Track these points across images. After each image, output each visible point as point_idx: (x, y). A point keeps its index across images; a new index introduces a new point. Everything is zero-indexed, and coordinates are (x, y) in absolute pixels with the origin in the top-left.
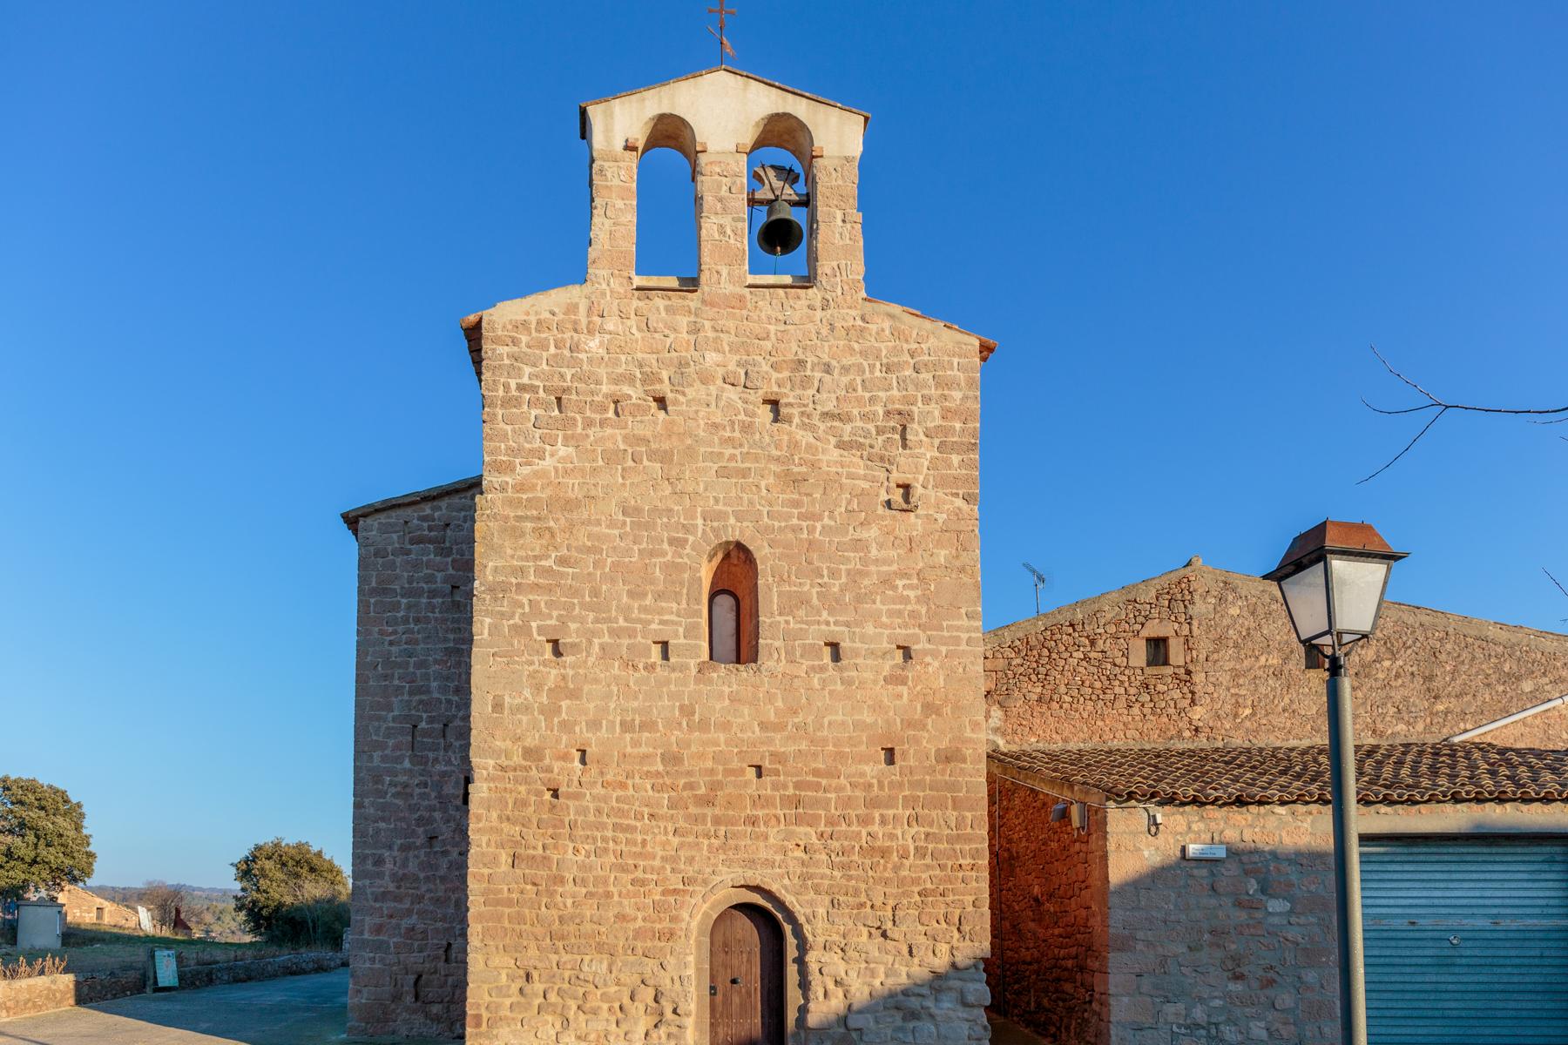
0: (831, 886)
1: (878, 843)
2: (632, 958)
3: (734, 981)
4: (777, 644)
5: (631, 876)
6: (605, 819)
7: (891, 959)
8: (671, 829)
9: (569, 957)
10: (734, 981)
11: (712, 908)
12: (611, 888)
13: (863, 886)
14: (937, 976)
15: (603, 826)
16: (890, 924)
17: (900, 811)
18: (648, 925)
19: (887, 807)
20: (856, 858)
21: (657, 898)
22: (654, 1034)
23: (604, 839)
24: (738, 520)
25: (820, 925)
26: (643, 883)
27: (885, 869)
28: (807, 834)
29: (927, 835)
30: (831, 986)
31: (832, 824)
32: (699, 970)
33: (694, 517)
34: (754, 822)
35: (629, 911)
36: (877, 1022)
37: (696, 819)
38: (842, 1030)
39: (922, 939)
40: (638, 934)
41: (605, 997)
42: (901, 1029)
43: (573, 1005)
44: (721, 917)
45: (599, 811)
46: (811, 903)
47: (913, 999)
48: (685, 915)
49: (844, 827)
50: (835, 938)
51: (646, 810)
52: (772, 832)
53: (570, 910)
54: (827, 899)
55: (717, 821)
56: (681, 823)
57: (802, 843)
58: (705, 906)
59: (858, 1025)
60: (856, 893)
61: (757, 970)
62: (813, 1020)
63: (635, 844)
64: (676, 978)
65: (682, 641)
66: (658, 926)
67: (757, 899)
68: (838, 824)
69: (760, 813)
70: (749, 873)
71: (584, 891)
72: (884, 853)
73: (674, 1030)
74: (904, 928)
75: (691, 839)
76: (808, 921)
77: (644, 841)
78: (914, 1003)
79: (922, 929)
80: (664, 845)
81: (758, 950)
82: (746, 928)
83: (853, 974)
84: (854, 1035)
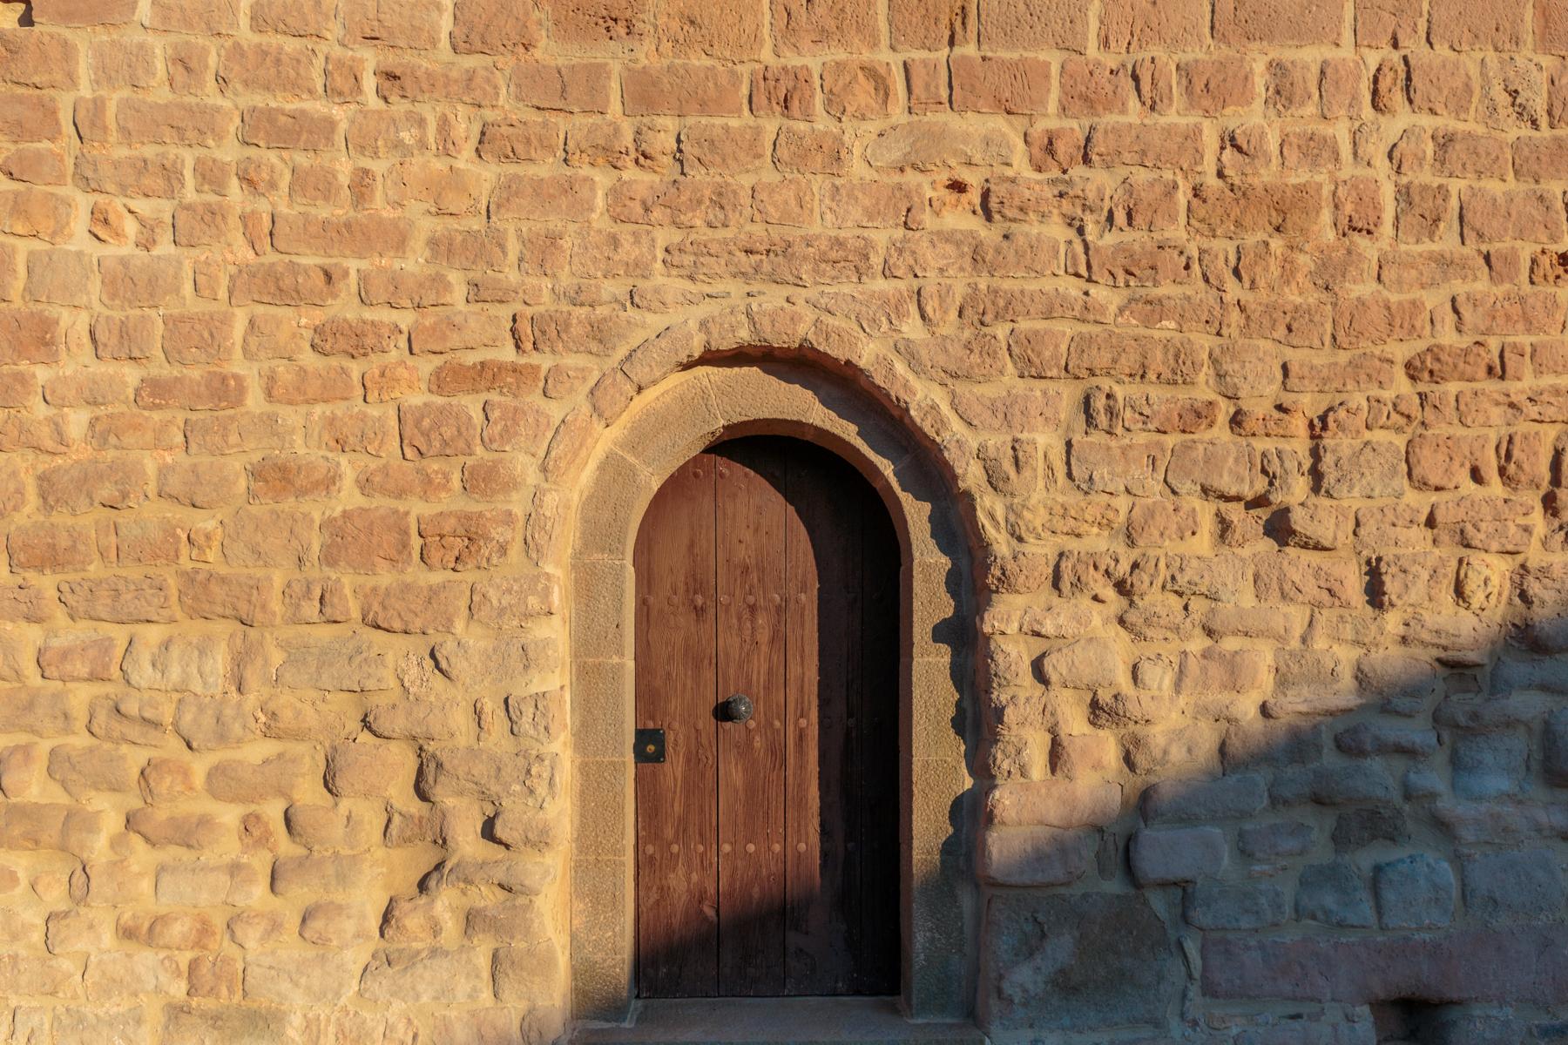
0: (1082, 344)
1: (1266, 175)
2: (323, 634)
3: (724, 712)
5: (310, 317)
6: (210, 95)
7: (1297, 616)
8: (465, 127)
9: (83, 631)
10: (724, 712)
11: (638, 440)
12: (237, 365)
13: (1204, 342)
14: (1455, 668)
15: (200, 125)
16: (1299, 487)
17: (1347, 52)
18: (382, 503)
19: (1300, 34)
20: (1176, 232)
21: (416, 399)
22: (412, 920)
23: (210, 176)
25: (1039, 495)
26: (358, 342)
27: (1288, 271)
28: (986, 138)
29: (1445, 142)
30: (1075, 723)
32: (588, 675)
34: (786, 96)
35: (304, 449)
36: (1245, 853)
38: (1114, 886)
39: (1418, 537)
40: (343, 541)
41: (222, 782)
42: (1331, 876)
43: (108, 811)
44: (676, 488)
45: (184, 63)
46: (1005, 412)
47: (1376, 764)
48: (524, 465)
49: (1134, 112)
50: (1098, 542)
51: (370, 59)
52: (859, 137)
53: (81, 453)
54: (1067, 395)
55: (645, 94)
56: (506, 106)
57: (973, 178)
58: (605, 440)
59: (1179, 871)
60: (1178, 376)
61: (806, 670)
62: (1005, 844)
63: (323, 187)
64: (491, 706)
66: (417, 508)
67: (801, 405)
68: (1113, 102)
69: (813, 60)
70: (771, 299)
71: (132, 375)
72: (1285, 212)
73: (486, 897)
74: (1351, 500)
75: (546, 168)
76: (994, 481)
77: (362, 185)
78: (1379, 778)
79: (1420, 502)
80: (439, 195)
81: (809, 600)
82: (765, 526)
83: (1159, 678)
84: (1158, 903)
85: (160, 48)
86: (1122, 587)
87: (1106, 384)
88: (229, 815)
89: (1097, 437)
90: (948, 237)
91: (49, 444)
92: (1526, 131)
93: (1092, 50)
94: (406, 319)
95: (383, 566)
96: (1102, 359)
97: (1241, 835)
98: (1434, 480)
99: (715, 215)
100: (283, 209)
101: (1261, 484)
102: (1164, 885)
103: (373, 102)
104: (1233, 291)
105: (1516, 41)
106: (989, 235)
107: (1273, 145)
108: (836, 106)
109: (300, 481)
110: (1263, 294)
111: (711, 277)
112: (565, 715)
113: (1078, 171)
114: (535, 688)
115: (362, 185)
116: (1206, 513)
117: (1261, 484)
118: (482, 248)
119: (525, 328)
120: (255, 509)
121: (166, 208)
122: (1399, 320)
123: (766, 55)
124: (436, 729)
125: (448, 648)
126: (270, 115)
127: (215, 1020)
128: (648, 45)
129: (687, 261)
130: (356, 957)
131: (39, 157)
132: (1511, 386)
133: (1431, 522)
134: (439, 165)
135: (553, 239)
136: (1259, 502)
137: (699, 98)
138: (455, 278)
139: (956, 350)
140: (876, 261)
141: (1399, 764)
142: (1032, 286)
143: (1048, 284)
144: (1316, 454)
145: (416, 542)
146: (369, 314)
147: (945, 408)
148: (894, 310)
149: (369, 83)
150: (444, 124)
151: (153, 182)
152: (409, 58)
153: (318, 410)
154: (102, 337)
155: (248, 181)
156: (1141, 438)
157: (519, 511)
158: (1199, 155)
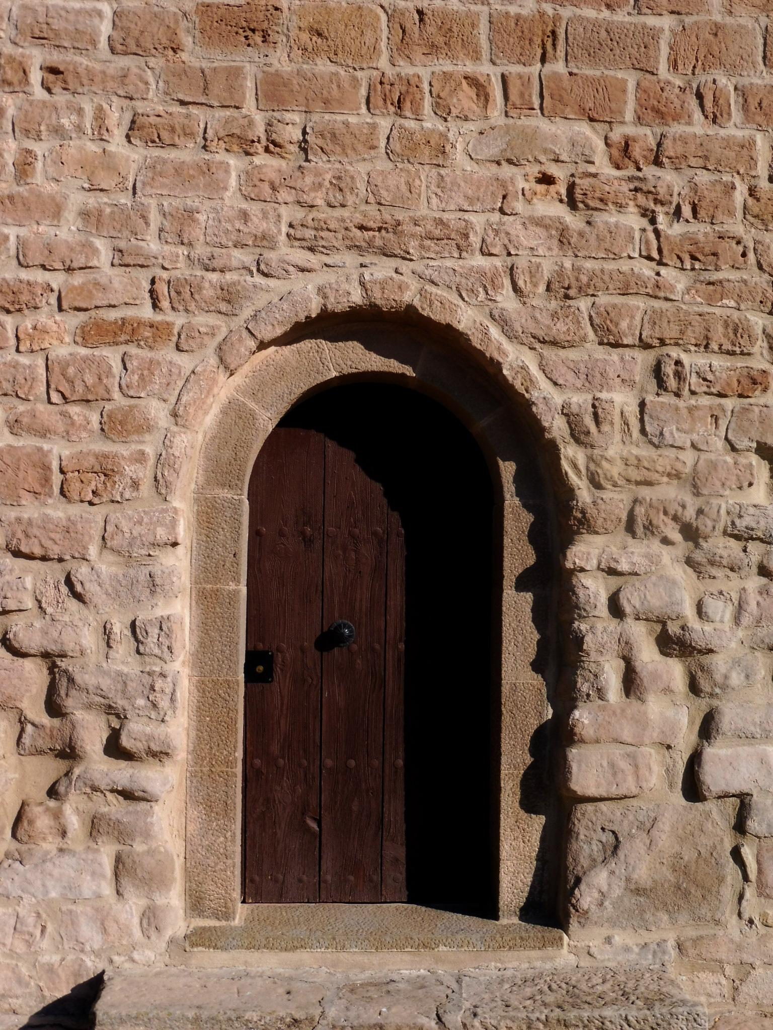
0: (655, 318)
8: (117, 118)
20: (736, 227)
25: (616, 448)
30: (647, 655)
31: (661, 115)
32: (207, 599)
34: (399, 98)
37: (204, 88)
48: (157, 411)
50: (669, 492)
51: (37, 57)
54: (642, 360)
58: (226, 388)
64: (119, 628)
66: (58, 450)
67: (354, 358)
70: (381, 270)
86: (691, 533)
87: (675, 353)
89: (667, 399)
90: (539, 222)
94: (57, 280)
95: (27, 499)
96: (671, 332)
103: (39, 93)
106: (573, 221)
108: (442, 110)
111: (329, 249)
112: (185, 638)
113: (650, 171)
114: (160, 612)
123: (383, 62)
124: (70, 647)
125: (82, 572)
134: (93, 148)
135: (190, 214)
139: (545, 319)
140: (475, 240)
143: (625, 266)
145: (56, 479)
146: (24, 275)
147: (534, 370)
149: (36, 76)
150: (100, 116)
156: (705, 401)
157: (150, 450)
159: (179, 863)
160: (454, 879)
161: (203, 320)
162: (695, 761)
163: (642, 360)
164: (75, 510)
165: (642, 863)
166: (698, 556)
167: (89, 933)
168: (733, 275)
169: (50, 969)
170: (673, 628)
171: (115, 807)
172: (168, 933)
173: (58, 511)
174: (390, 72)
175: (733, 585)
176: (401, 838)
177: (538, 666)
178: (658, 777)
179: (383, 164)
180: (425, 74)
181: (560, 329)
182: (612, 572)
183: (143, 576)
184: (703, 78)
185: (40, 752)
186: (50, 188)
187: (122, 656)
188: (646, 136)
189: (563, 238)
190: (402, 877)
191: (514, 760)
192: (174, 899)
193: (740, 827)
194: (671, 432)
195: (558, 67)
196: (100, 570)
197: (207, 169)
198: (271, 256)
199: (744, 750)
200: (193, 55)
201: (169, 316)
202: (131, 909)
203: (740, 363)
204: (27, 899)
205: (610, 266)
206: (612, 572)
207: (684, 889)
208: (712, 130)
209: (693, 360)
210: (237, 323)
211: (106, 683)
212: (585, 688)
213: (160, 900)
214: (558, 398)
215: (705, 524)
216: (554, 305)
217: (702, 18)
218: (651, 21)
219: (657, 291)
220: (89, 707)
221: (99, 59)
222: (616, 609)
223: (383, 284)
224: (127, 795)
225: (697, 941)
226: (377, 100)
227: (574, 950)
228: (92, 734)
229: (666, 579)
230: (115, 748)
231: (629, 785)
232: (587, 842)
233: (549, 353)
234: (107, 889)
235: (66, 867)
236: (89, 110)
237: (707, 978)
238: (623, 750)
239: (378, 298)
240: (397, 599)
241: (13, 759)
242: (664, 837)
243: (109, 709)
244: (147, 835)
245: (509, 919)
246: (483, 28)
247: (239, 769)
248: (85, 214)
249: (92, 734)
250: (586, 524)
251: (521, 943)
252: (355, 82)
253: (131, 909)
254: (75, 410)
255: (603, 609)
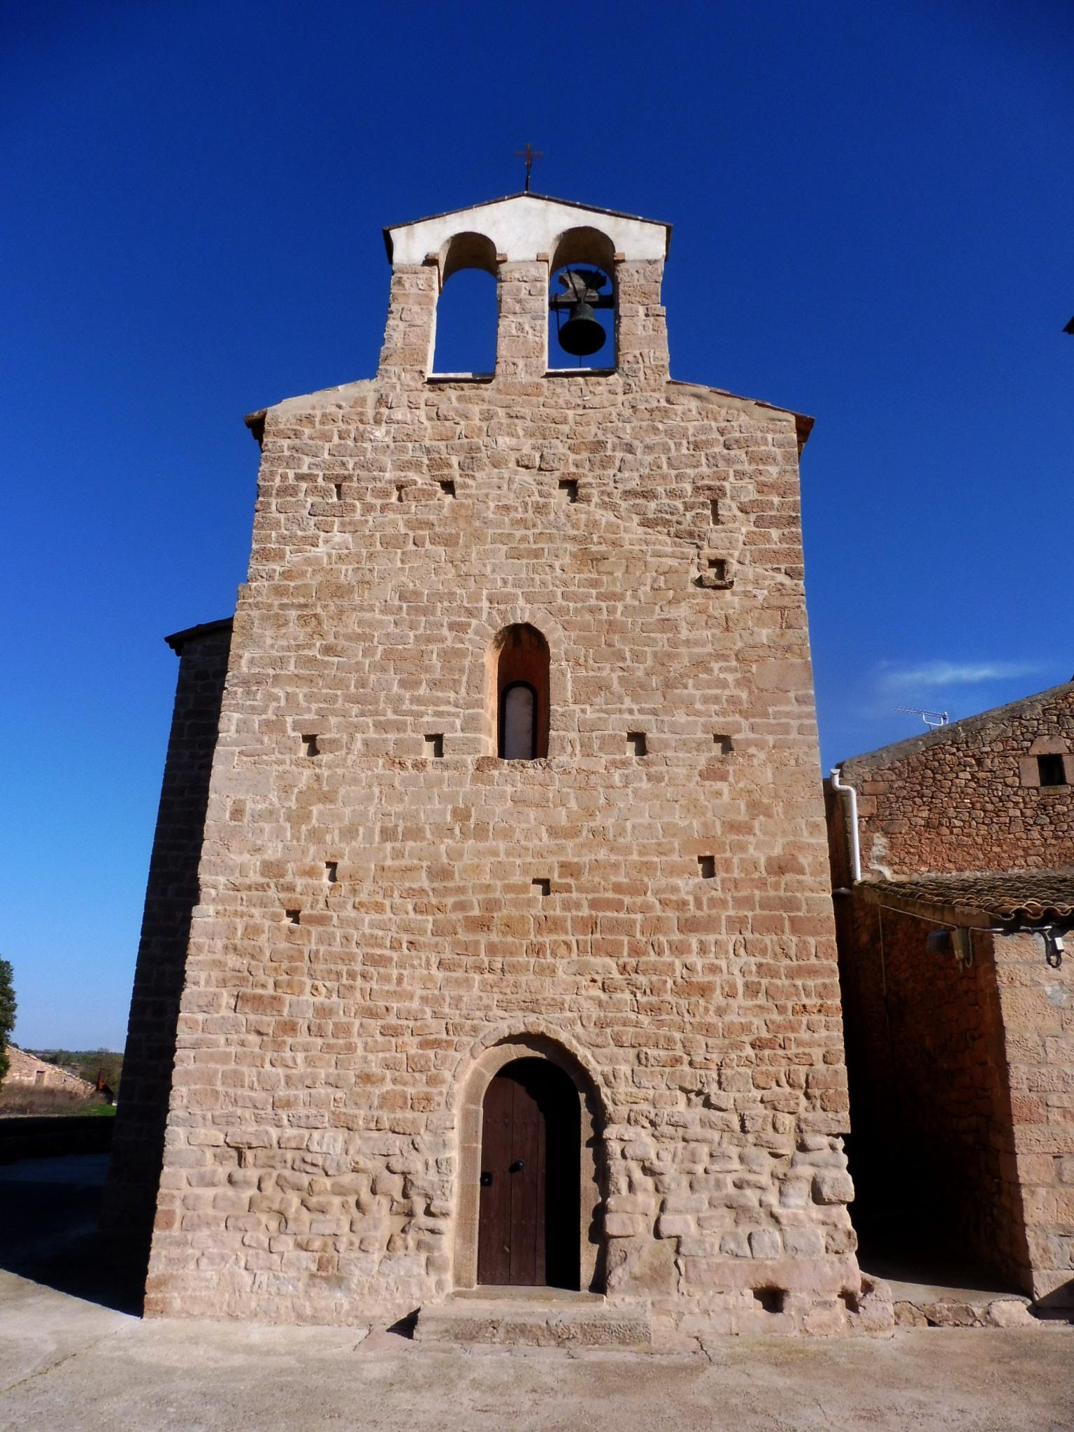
0: (636, 1035)
4: (573, 735)
8: (434, 960)
11: (486, 1064)
13: (678, 1036)
16: (715, 1086)
20: (668, 997)
23: (351, 975)
24: (528, 601)
25: (623, 1089)
27: (707, 1009)
29: (760, 966)
32: (466, 1150)
33: (478, 600)
34: (538, 950)
35: (375, 1069)
36: (699, 1224)
40: (386, 1101)
41: (339, 1190)
48: (447, 1075)
50: (644, 1107)
51: (405, 938)
54: (632, 1053)
58: (473, 1064)
63: (387, 979)
64: (432, 1162)
65: (459, 734)
66: (410, 1091)
67: (524, 1051)
68: (645, 953)
70: (532, 1018)
72: (704, 990)
77: (400, 980)
80: (427, 981)
85: (338, 934)
86: (653, 1123)
87: (645, 1049)
88: (337, 1201)
89: (642, 1068)
90: (591, 998)
91: (291, 1065)
92: (788, 962)
93: (638, 935)
94: (411, 1024)
95: (398, 1110)
96: (642, 1041)
97: (699, 1219)
98: (762, 1085)
99: (515, 990)
100: (375, 987)
101: (700, 1086)
102: (670, 1237)
103: (406, 951)
104: (687, 1018)
105: (783, 932)
106: (604, 996)
107: (699, 968)
108: (554, 954)
109: (373, 1079)
110: (698, 1019)
111: (512, 1010)
112: (456, 1167)
113: (634, 976)
114: (447, 1155)
115: (400, 980)
116: (682, 1097)
117: (700, 1086)
118: (438, 1001)
119: (450, 1027)
120: (357, 1089)
121: (336, 984)
122: (745, 1028)
123: (532, 937)
124: (412, 1170)
125: (418, 1139)
126: (373, 955)
127: (326, 1279)
128: (494, 934)
129: (505, 1006)
130: (376, 1257)
131: (297, 968)
132: (788, 1052)
133: (762, 1101)
134: (425, 972)
135: (460, 998)
136: (699, 1093)
137: (510, 951)
138: (428, 1010)
139: (594, 1036)
140: (566, 1006)
141: (758, 1192)
142: (619, 1015)
143: (624, 1015)
144: (719, 1075)
145: (410, 1102)
146: (400, 1022)
147: (590, 1057)
148: (572, 1023)
149: (405, 945)
150: (428, 960)
151: (333, 976)
152: (417, 937)
153: (381, 1055)
154: (312, 1028)
155: (363, 977)
156: (658, 1069)
157: (444, 1091)
158: (674, 971)
159: (451, 1263)
160: (563, 1274)
161: (465, 1039)
162: (658, 1221)
163: (632, 1053)
164: (416, 1114)
165: (636, 1265)
166: (656, 1133)
167: (415, 1291)
168: (667, 1017)
169: (399, 1306)
170: (647, 1164)
171: (427, 1237)
172: (446, 1292)
173: (409, 1115)
174: (535, 941)
175: (671, 1146)
176: (544, 1257)
177: (595, 1179)
178: (643, 1228)
179: (532, 977)
180: (547, 940)
181: (599, 1041)
182: (622, 1140)
183: (441, 1141)
184: (654, 938)
185: (398, 1214)
186: (409, 988)
187: (433, 1175)
188: (632, 961)
189: (600, 1004)
190: (544, 1273)
191: (586, 1220)
192: (449, 1277)
193: (677, 1252)
194: (645, 1083)
195: (598, 936)
196: (425, 1138)
197: (467, 980)
198: (490, 1013)
199: (678, 1217)
200: (462, 936)
201: (453, 1038)
202: (431, 1281)
203: (671, 1053)
204: (392, 1276)
205: (619, 1015)
206: (622, 1140)
207: (655, 1278)
208: (658, 958)
209: (652, 1052)
210: (478, 1040)
211: (426, 1185)
212: (613, 1189)
213: (444, 1277)
214: (599, 1068)
215: (658, 1120)
216: (597, 1030)
217: (653, 914)
218: (633, 916)
219: (637, 1024)
220: (419, 1194)
221: (427, 938)
222: (624, 1156)
223: (532, 1024)
224: (432, 1231)
225: (660, 1302)
226: (530, 951)
227: (608, 1303)
228: (420, 1207)
229: (643, 1142)
230: (428, 1212)
231: (630, 1231)
232: (614, 1256)
233: (595, 1049)
234: (423, 1272)
235: (407, 1262)
236: (424, 958)
237: (664, 1319)
238: (629, 1215)
239: (530, 1030)
240: (542, 1150)
241: (388, 1216)
242: (645, 1254)
243: (427, 1196)
244: (439, 1249)
245: (584, 1291)
246: (569, 923)
247: (477, 1222)
248: (422, 998)
249: (420, 1207)
250: (611, 1120)
251: (585, 1299)
252: (521, 945)
253: (431, 1281)
254: (417, 1075)
255: (619, 1155)
